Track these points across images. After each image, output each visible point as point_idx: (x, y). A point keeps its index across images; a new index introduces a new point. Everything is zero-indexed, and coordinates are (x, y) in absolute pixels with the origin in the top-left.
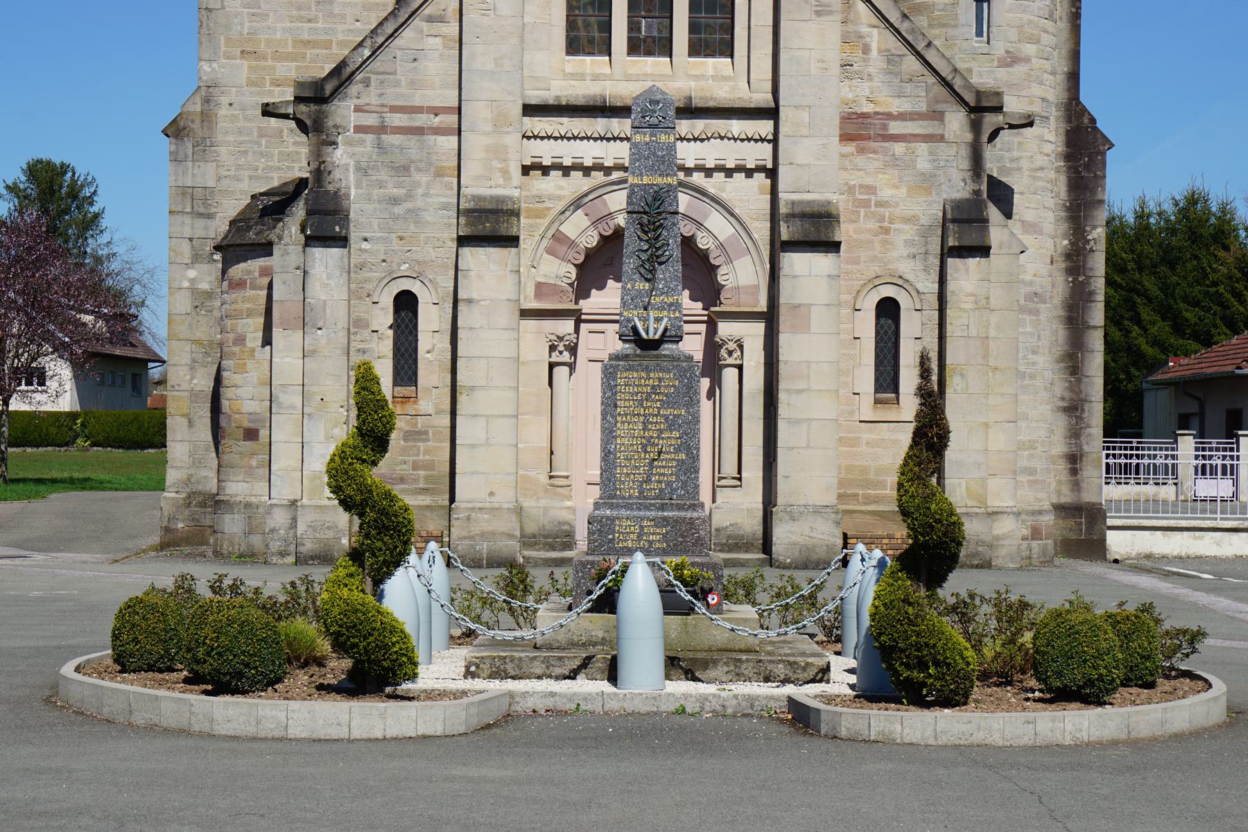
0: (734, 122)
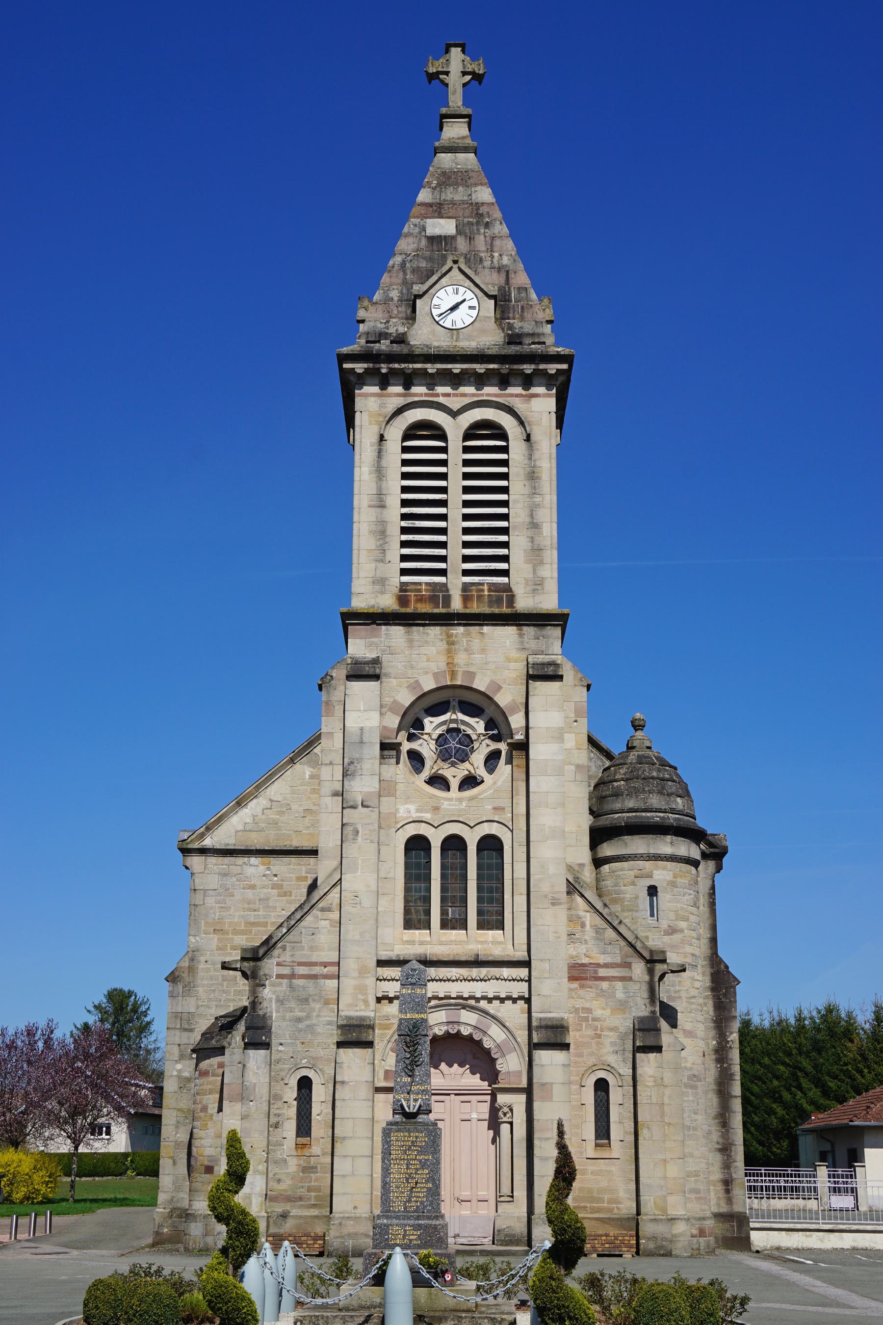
0: (505, 969)
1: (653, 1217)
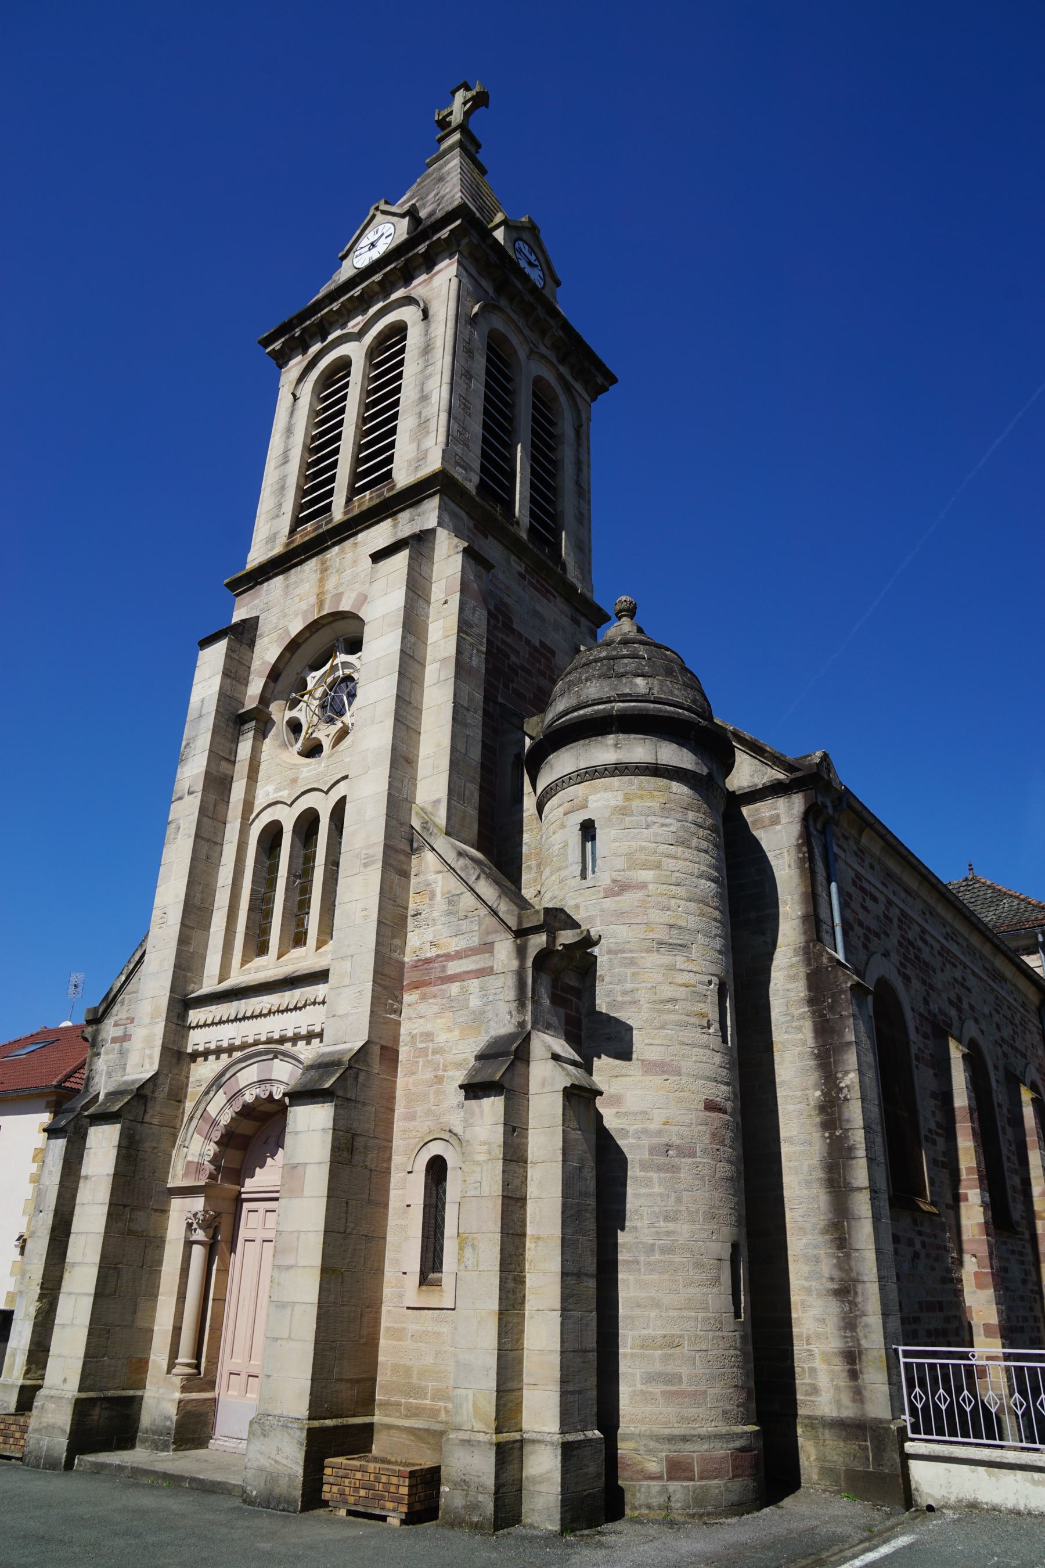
1: (466, 1436)
